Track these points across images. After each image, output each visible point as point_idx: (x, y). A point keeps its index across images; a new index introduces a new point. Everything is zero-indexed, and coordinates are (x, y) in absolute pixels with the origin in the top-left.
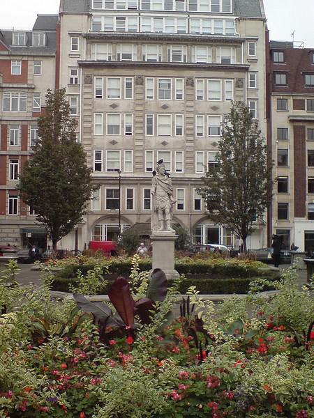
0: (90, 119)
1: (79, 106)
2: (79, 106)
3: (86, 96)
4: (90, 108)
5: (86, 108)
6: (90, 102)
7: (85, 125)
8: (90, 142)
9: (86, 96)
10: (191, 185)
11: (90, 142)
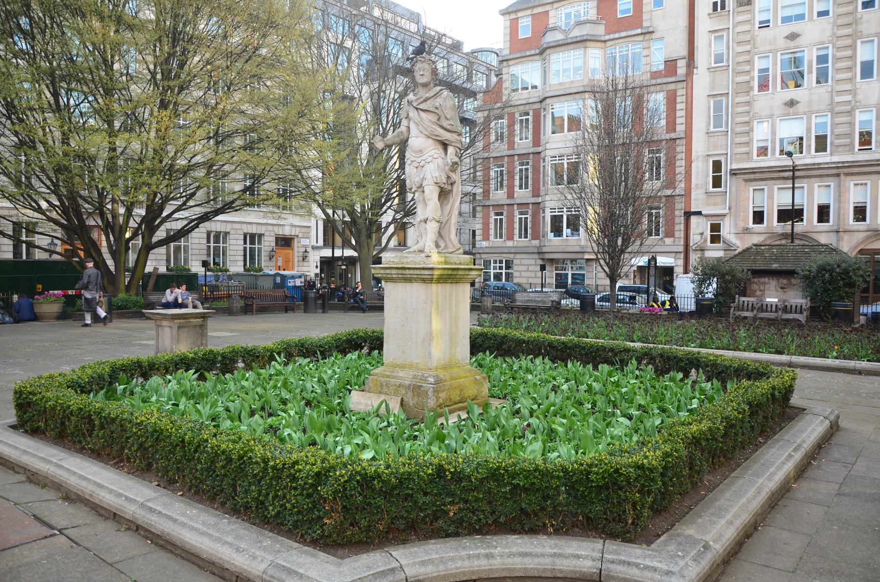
0: (747, 68)
1: (728, 48)
2: (728, 48)
3: (740, 29)
4: (748, 48)
5: (740, 49)
6: (747, 37)
7: (739, 79)
8: (747, 108)
9: (740, 29)
10: (847, 174)
11: (747, 108)
